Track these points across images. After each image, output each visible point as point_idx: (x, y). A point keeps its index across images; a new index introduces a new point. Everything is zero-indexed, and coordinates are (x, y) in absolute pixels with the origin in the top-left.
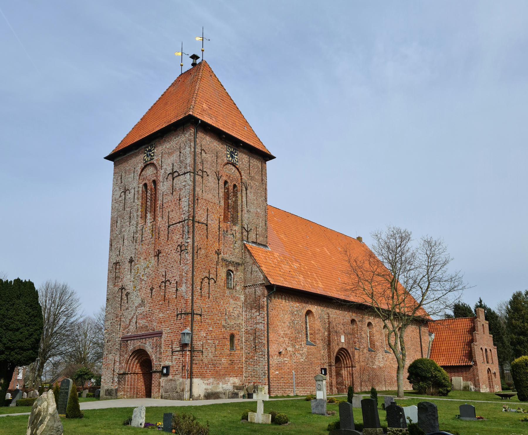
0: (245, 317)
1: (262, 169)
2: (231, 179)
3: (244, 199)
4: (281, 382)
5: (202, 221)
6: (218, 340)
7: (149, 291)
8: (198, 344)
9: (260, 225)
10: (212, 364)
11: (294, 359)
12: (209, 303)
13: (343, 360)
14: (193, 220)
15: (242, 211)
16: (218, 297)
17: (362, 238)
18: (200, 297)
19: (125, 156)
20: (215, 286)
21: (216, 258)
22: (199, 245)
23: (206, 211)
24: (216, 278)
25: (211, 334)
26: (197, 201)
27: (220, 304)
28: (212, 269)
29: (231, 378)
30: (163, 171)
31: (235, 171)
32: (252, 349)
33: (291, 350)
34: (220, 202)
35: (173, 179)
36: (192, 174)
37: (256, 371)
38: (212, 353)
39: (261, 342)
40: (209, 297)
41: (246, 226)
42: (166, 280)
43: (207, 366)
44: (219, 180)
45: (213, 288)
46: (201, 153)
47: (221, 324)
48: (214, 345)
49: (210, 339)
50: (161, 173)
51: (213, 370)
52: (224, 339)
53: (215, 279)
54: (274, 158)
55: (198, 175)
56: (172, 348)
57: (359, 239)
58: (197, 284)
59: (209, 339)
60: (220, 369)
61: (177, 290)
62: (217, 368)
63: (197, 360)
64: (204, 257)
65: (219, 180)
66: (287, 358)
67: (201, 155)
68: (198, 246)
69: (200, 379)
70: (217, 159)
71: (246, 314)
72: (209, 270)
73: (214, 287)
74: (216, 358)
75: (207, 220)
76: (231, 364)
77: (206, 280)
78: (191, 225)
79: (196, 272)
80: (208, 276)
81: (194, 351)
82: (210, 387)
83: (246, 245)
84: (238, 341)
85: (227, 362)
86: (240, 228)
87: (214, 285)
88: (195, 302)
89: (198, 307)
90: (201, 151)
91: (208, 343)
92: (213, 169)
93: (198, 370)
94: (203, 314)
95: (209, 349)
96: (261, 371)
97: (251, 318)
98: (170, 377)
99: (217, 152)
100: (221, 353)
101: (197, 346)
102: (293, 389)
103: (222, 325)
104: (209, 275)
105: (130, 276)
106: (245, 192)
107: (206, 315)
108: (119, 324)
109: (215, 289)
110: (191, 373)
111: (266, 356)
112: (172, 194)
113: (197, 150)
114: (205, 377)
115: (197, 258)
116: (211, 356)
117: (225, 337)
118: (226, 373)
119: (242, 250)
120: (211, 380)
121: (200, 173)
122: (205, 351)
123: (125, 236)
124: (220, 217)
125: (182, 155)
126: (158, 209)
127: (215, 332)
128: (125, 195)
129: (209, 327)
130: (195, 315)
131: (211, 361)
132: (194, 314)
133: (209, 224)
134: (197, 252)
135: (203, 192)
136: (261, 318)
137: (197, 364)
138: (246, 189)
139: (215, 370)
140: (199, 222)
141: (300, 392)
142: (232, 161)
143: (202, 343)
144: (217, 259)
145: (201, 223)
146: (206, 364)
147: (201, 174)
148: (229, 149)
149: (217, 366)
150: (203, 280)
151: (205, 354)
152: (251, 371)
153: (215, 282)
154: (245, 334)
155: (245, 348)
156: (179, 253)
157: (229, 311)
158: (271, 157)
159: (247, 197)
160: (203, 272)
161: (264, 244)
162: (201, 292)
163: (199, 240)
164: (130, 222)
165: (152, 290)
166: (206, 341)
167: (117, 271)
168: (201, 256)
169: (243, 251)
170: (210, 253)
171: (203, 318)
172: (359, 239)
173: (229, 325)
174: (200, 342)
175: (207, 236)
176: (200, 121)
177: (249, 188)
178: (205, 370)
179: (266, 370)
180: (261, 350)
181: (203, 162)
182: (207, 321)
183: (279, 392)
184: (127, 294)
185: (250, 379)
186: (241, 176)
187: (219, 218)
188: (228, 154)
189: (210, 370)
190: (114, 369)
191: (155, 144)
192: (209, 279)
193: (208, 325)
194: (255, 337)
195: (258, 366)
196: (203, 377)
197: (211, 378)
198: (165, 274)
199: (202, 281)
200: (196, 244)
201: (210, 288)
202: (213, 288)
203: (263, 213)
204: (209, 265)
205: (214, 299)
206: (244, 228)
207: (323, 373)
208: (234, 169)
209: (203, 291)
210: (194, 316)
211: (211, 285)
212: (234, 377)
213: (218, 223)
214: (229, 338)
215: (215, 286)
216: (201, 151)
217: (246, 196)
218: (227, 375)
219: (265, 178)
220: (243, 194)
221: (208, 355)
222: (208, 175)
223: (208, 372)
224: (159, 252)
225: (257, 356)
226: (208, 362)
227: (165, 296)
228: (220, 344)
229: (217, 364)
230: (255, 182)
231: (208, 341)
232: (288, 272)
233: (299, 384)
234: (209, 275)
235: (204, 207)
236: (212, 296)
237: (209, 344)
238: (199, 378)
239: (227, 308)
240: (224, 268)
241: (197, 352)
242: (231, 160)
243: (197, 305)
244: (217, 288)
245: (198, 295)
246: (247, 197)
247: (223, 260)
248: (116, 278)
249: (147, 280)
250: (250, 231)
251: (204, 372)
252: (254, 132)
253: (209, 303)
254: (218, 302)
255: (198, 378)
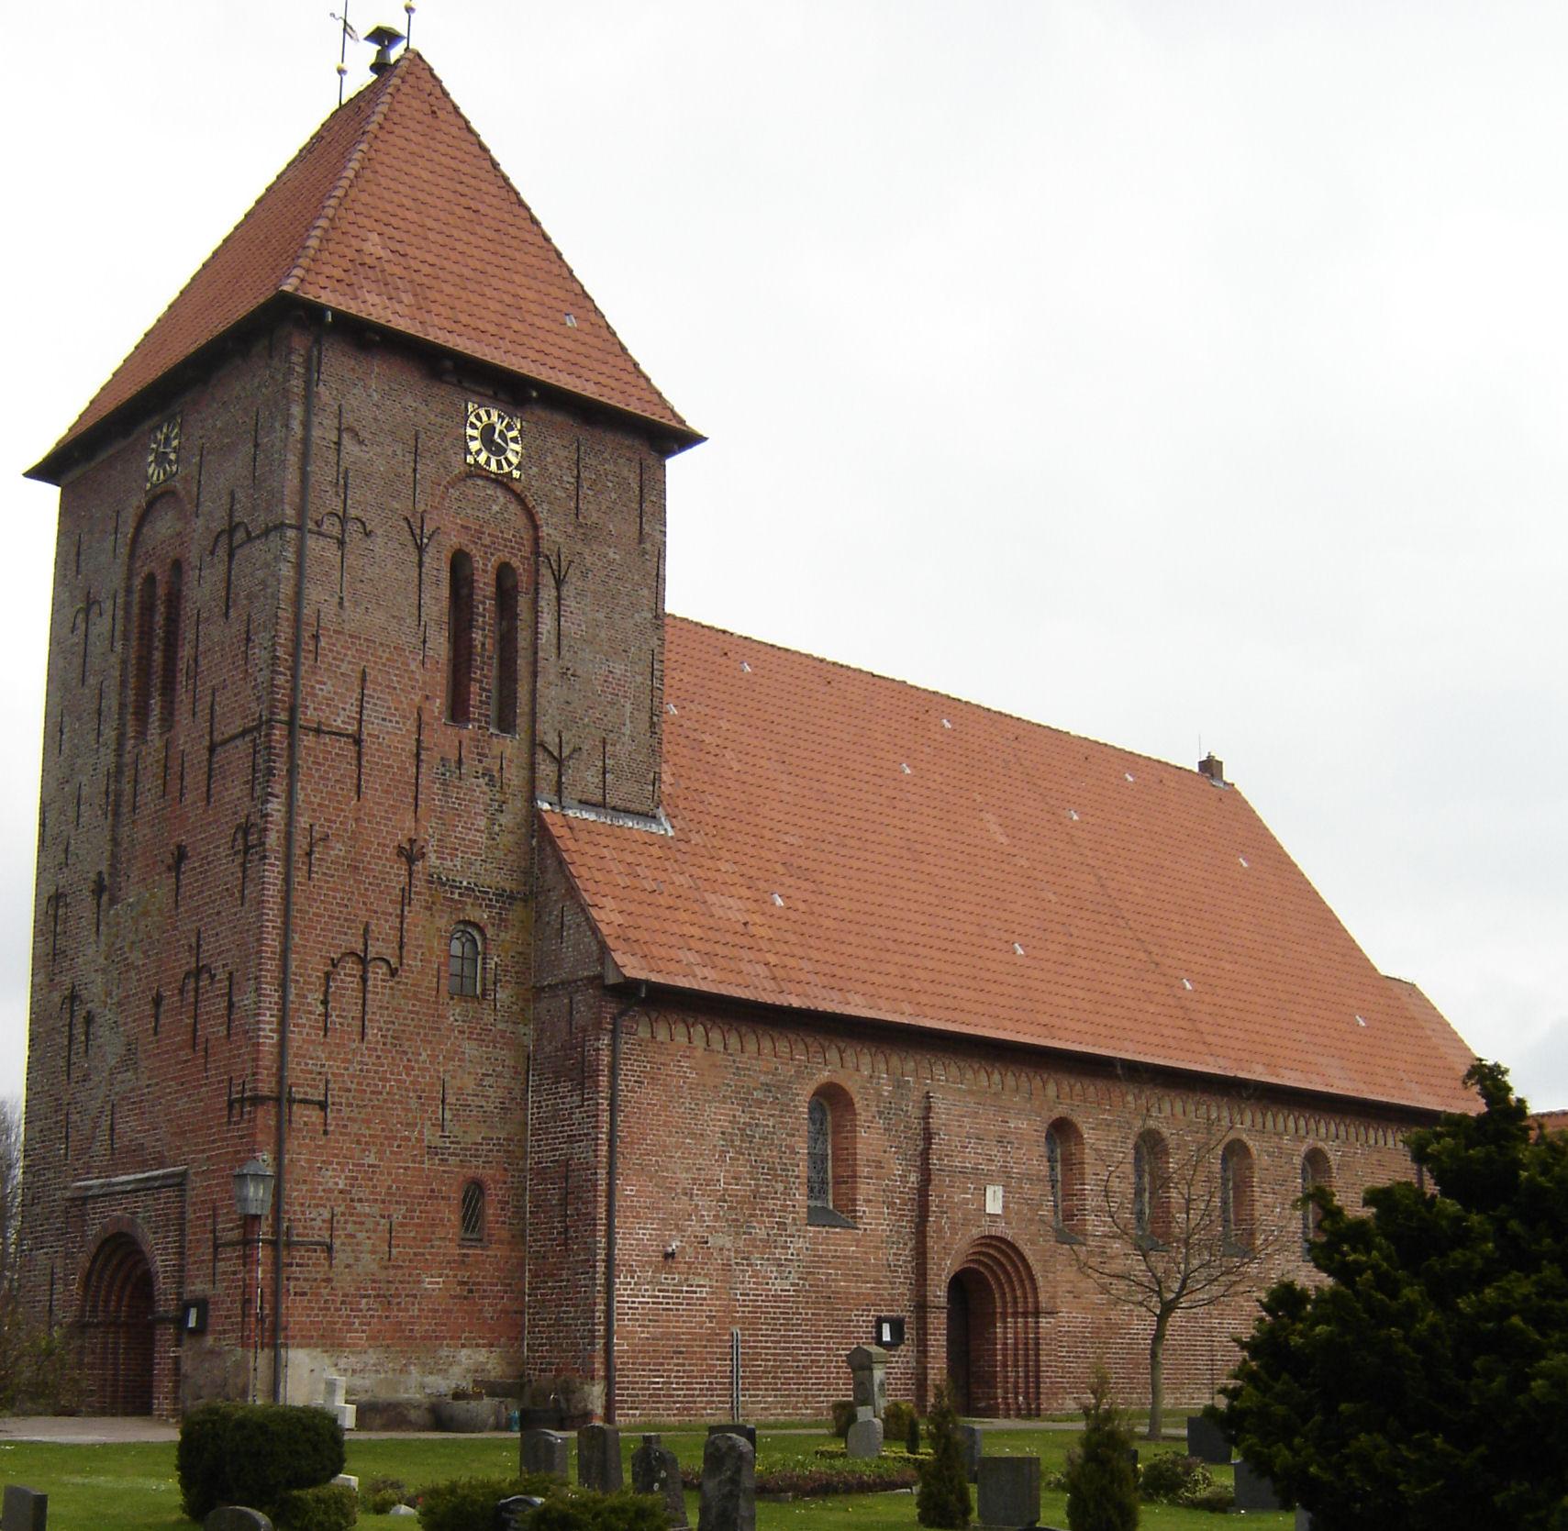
0: (533, 1114)
1: (641, 491)
2: (487, 541)
3: (547, 625)
4: (671, 1370)
5: (339, 723)
6: (405, 1203)
7: (149, 1009)
8: (308, 1218)
9: (627, 730)
10: (378, 1296)
11: (742, 1282)
12: (362, 1055)
13: (1000, 1285)
14: (291, 723)
15: (535, 674)
16: (408, 1035)
17: (1221, 763)
18: (322, 1033)
19: (93, 464)
20: (391, 988)
21: (399, 875)
22: (321, 826)
23: (357, 682)
24: (401, 958)
25: (371, 1179)
26: (311, 642)
27: (417, 1061)
28: (378, 919)
29: (464, 1352)
30: (200, 522)
31: (504, 509)
32: (554, 1240)
33: (729, 1245)
34: (424, 642)
35: (231, 556)
36: (291, 533)
37: (566, 1325)
38: (373, 1252)
39: (584, 1214)
40: (363, 1035)
41: (551, 739)
42: (200, 965)
43: (350, 1303)
44: (421, 549)
45: (386, 998)
46: (338, 444)
47: (420, 1140)
48: (383, 1221)
49: (367, 1200)
50: (194, 531)
51: (380, 1317)
52: (436, 1198)
53: (392, 961)
54: (706, 439)
55: (320, 534)
56: (214, 1231)
57: (1210, 767)
58: (305, 982)
59: (360, 1200)
60: (412, 1317)
61: (231, 1005)
62: (399, 1310)
63: (306, 1280)
64: (344, 871)
65: (421, 549)
66: (706, 1275)
67: (339, 451)
68: (317, 828)
69: (319, 1350)
70: (415, 462)
71: (540, 1102)
72: (367, 924)
73: (387, 991)
74: (392, 1272)
75: (360, 721)
76: (465, 1298)
77: (351, 966)
78: (285, 745)
79: (302, 933)
80: (362, 947)
81: (289, 1245)
82: (367, 1382)
83: (548, 819)
84: (503, 1209)
85: (448, 1290)
86: (525, 747)
87: (390, 983)
88: (296, 1055)
89: (311, 1073)
90: (340, 437)
91: (358, 1215)
92: (396, 505)
93: (309, 1316)
94: (337, 1100)
95: (361, 1236)
96: (582, 1324)
97: (553, 1116)
98: (209, 1341)
99: (417, 432)
100: (415, 1254)
101: (305, 1228)
102: (731, 1396)
103: (426, 1143)
104: (366, 945)
105: (94, 946)
106: (554, 593)
107: (350, 1105)
108: (64, 1134)
109: (395, 1003)
110: (276, 1328)
111: (601, 1268)
112: (226, 615)
113: (316, 433)
114: (340, 1345)
115: (309, 878)
116: (369, 1263)
117: (440, 1191)
118: (441, 1331)
119: (533, 837)
120: (372, 1357)
121: (332, 527)
122: (343, 1244)
123: (83, 787)
124: (427, 705)
125: (261, 456)
126: (181, 678)
127: (390, 1174)
128: (87, 624)
129: (364, 1150)
130: (295, 1107)
131: (369, 1285)
132: (292, 1101)
133: (369, 735)
134: (309, 854)
135: (346, 604)
136: (588, 1117)
137: (304, 1294)
138: (559, 583)
139: (387, 1317)
140: (318, 731)
141: (765, 1409)
142: (493, 467)
143: (327, 1215)
144: (404, 879)
145: (329, 733)
146: (345, 1295)
147: (336, 531)
148: (479, 418)
149: (399, 1303)
150: (334, 966)
151: (340, 1258)
152: (549, 1326)
153: (393, 972)
154: (531, 1180)
155: (531, 1235)
156: (239, 860)
157: (459, 1088)
158: (687, 439)
159: (559, 616)
160: (339, 932)
161: (644, 808)
162: (326, 1015)
163: (319, 805)
164: (99, 735)
165: (157, 1001)
166: (347, 1207)
167: (58, 929)
168: (328, 868)
169: (534, 842)
170: (372, 856)
171: (334, 1118)
172: (1210, 767)
173: (458, 1143)
174: (321, 1210)
175: (359, 786)
176: (329, 313)
177: (573, 578)
178: (340, 1317)
179: (600, 1324)
180: (586, 1243)
181: (346, 478)
182: (353, 1128)
183: (658, 1409)
184: (89, 1019)
185: (545, 1358)
186: (536, 528)
187: (420, 710)
188: (473, 438)
189: (365, 1317)
190: (50, 1306)
191: (181, 412)
192: (363, 961)
193: (358, 1142)
194: (567, 1193)
195: (573, 1306)
196: (332, 1346)
197: (371, 1350)
198: (198, 941)
199: (330, 968)
200: (303, 821)
201: (369, 996)
202: (386, 998)
203: (639, 679)
204: (364, 903)
205: (389, 1040)
206: (542, 745)
207: (886, 1337)
208: (502, 500)
209: (334, 1009)
210: (290, 1109)
211: (375, 986)
212: (478, 1345)
213: (414, 729)
214: (456, 1196)
215: (391, 988)
216: (340, 437)
217: (559, 611)
218: (445, 1338)
219: (658, 527)
220: (542, 603)
221: (357, 1259)
222: (368, 534)
223: (357, 1325)
224: (181, 855)
225: (569, 1269)
226: (358, 1289)
227: (195, 1031)
228: (412, 1218)
229: (399, 1296)
230: (604, 549)
231: (357, 1205)
232: (740, 928)
233: (761, 1378)
234: (366, 945)
235: (345, 667)
236: (380, 1029)
237: (363, 1219)
238: (316, 1346)
239: (447, 1078)
240: (437, 915)
241: (307, 1251)
242: (488, 462)
243: (307, 1064)
244: (405, 997)
245: (311, 1027)
246: (559, 616)
247: (434, 880)
248: (55, 955)
249: (143, 965)
250: (570, 757)
251: (338, 1326)
252: (614, 334)
253: (362, 1055)
254: (405, 1053)
255: (308, 1345)
